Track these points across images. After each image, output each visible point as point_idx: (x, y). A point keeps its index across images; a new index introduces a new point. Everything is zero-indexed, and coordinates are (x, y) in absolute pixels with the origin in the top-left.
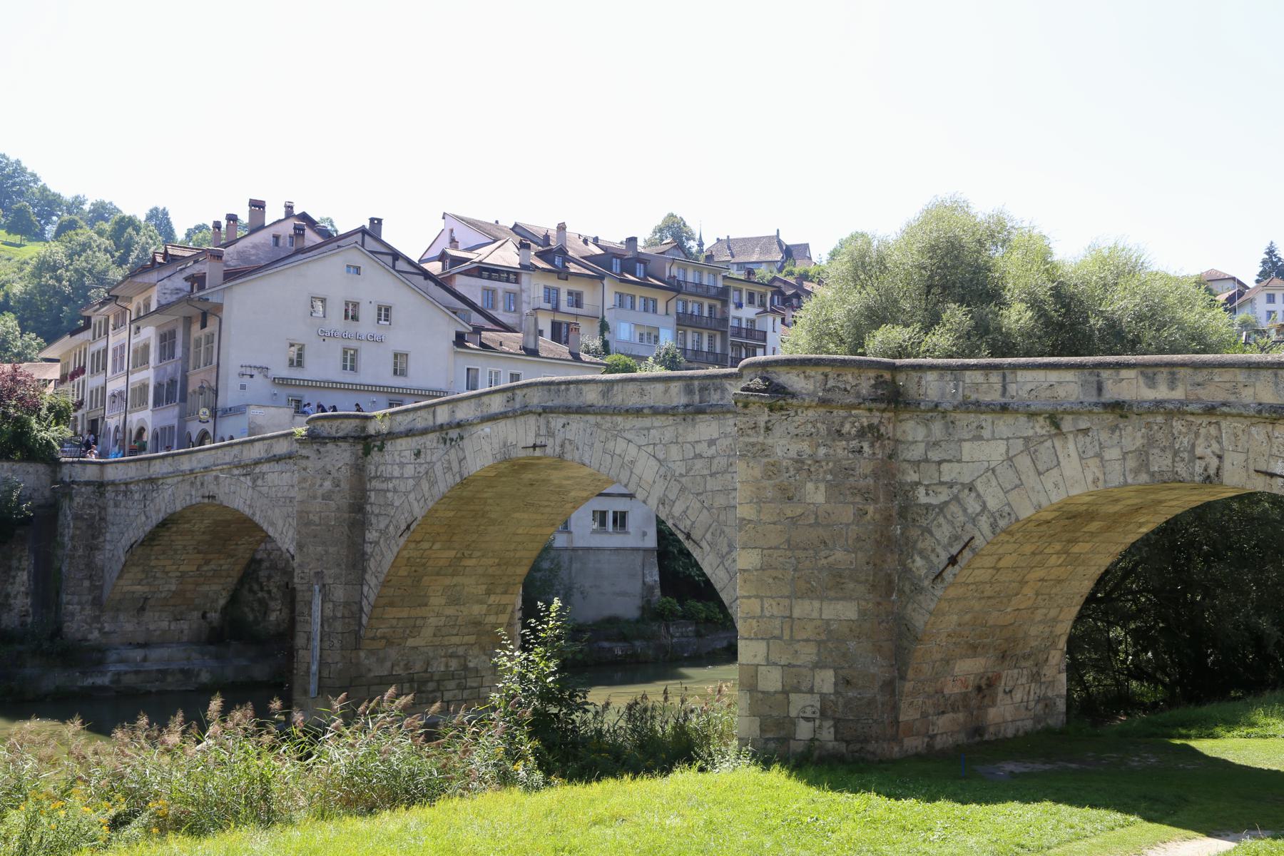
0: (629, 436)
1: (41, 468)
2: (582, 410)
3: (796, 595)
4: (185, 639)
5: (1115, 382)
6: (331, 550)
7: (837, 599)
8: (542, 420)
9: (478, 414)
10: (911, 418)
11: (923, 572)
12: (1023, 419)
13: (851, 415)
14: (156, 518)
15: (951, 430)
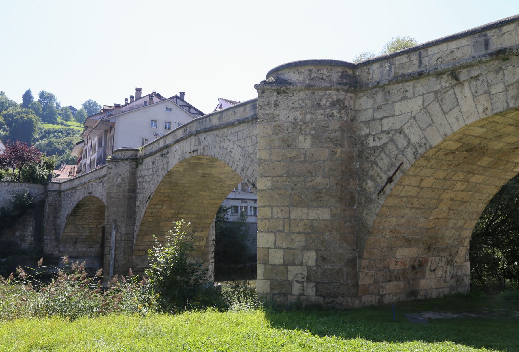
0: (229, 138)
1: (41, 186)
2: (211, 129)
3: (293, 205)
4: (93, 256)
5: (499, 36)
6: (120, 210)
7: (317, 207)
9: (174, 140)
10: (364, 95)
11: (372, 190)
12: (433, 79)
13: (326, 94)
14: (75, 204)
15: (387, 97)
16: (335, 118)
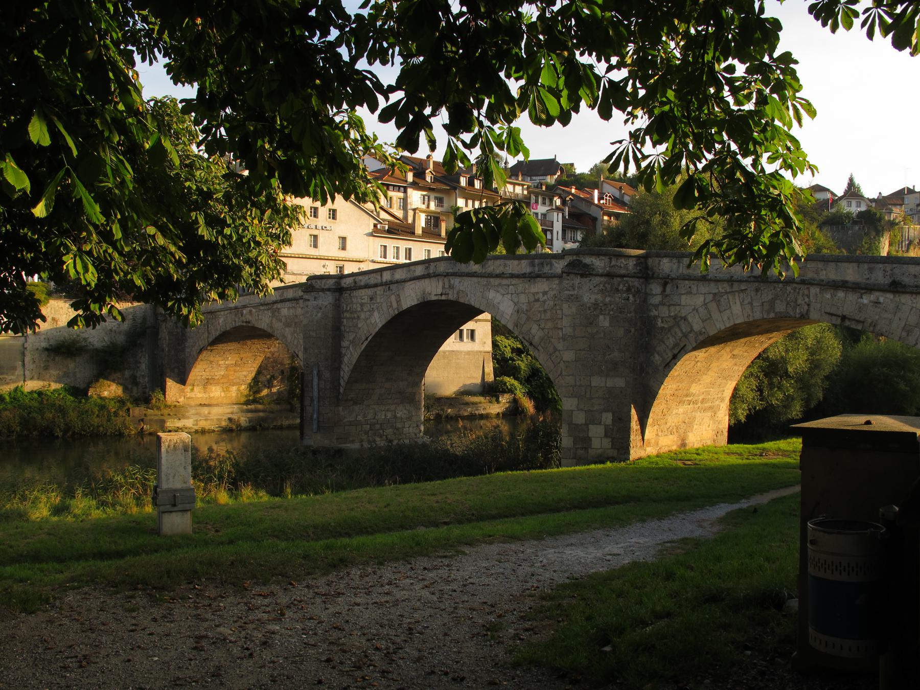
8: (446, 280)
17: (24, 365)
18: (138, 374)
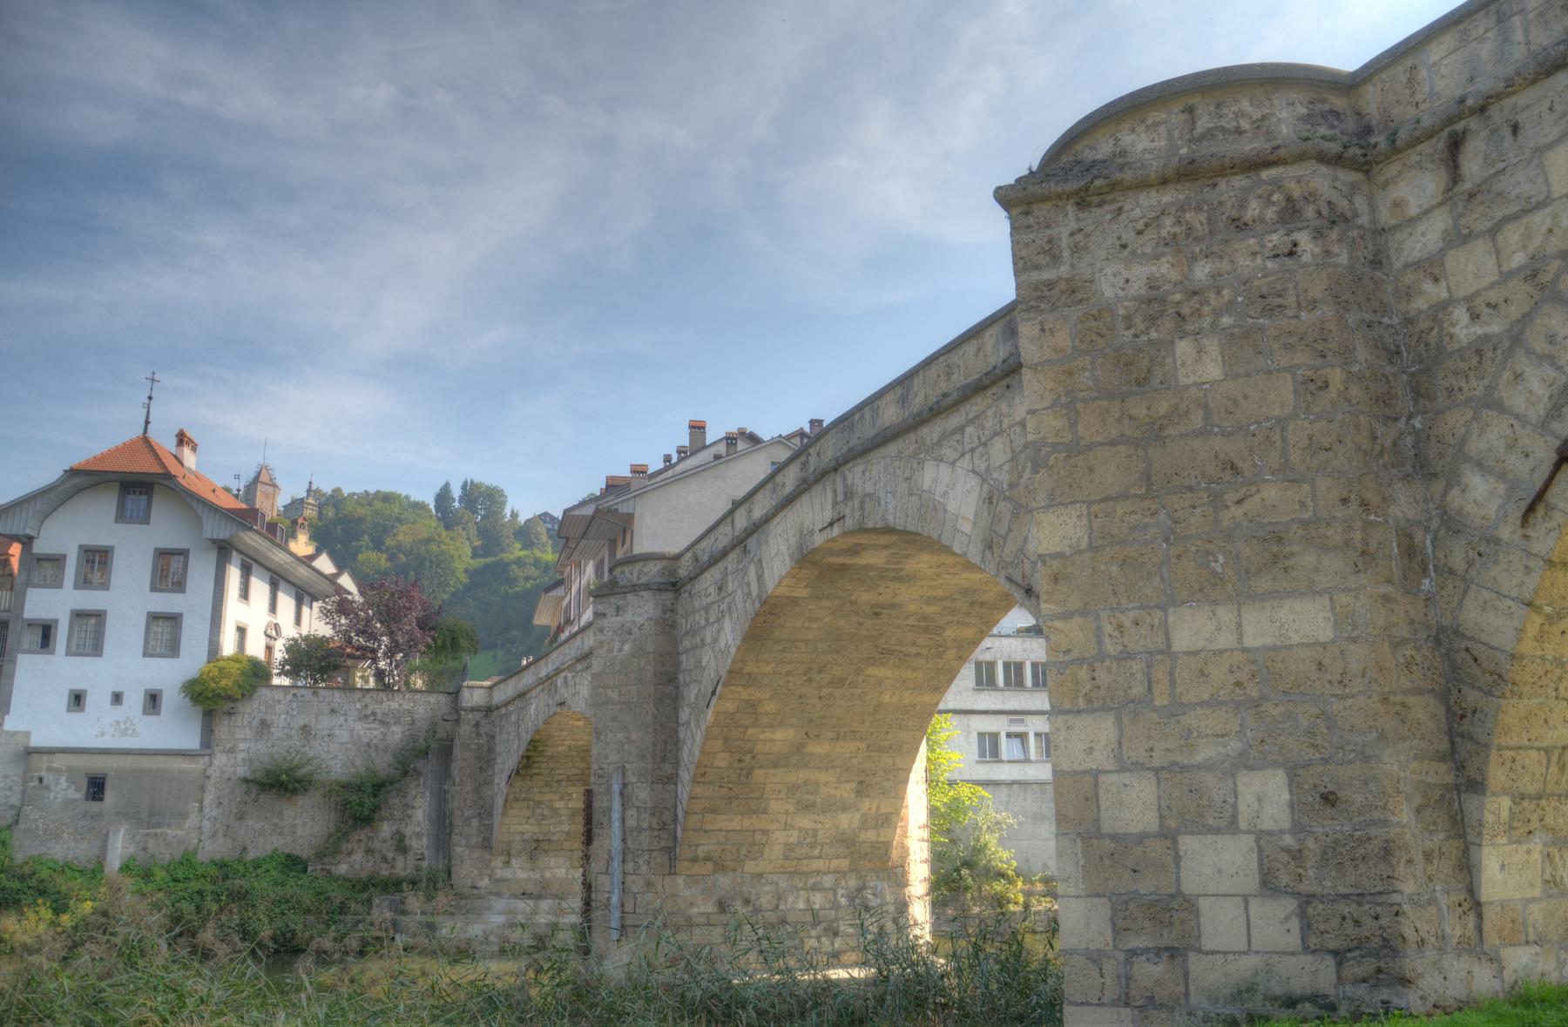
6: (634, 737)
16: (1306, 258)
17: (201, 809)
18: (409, 830)
